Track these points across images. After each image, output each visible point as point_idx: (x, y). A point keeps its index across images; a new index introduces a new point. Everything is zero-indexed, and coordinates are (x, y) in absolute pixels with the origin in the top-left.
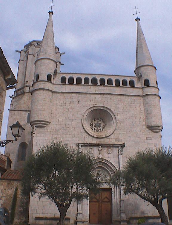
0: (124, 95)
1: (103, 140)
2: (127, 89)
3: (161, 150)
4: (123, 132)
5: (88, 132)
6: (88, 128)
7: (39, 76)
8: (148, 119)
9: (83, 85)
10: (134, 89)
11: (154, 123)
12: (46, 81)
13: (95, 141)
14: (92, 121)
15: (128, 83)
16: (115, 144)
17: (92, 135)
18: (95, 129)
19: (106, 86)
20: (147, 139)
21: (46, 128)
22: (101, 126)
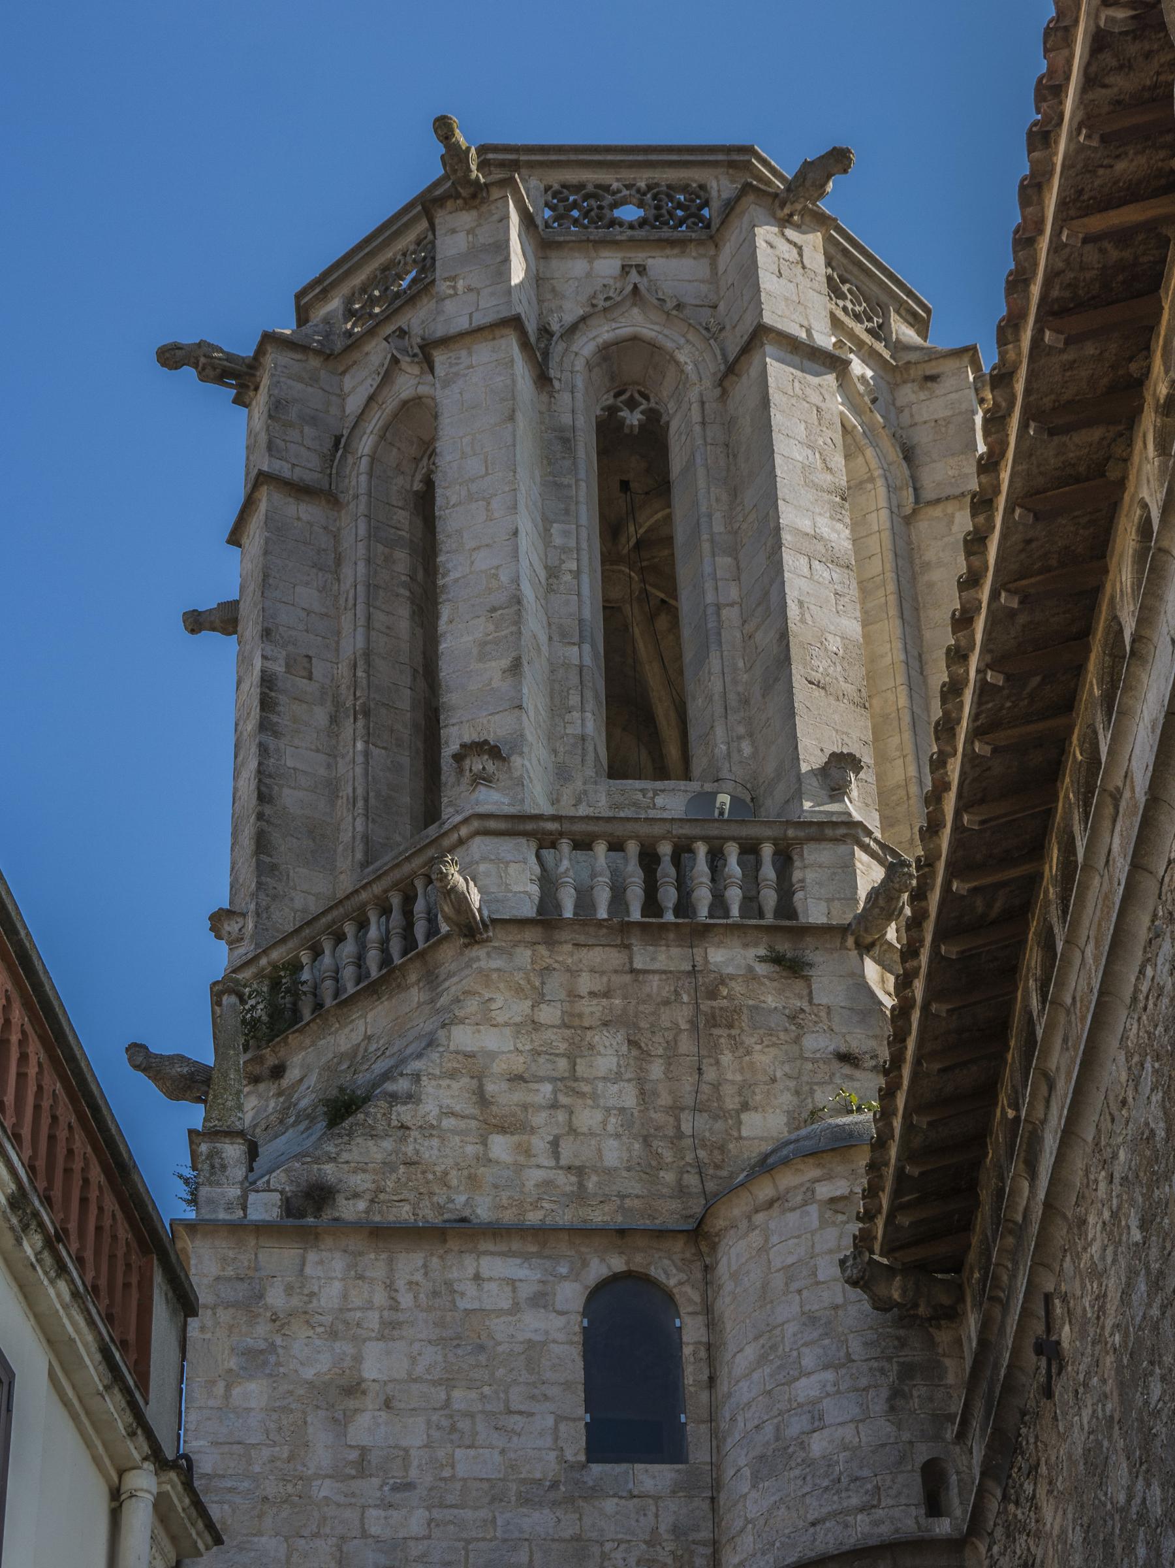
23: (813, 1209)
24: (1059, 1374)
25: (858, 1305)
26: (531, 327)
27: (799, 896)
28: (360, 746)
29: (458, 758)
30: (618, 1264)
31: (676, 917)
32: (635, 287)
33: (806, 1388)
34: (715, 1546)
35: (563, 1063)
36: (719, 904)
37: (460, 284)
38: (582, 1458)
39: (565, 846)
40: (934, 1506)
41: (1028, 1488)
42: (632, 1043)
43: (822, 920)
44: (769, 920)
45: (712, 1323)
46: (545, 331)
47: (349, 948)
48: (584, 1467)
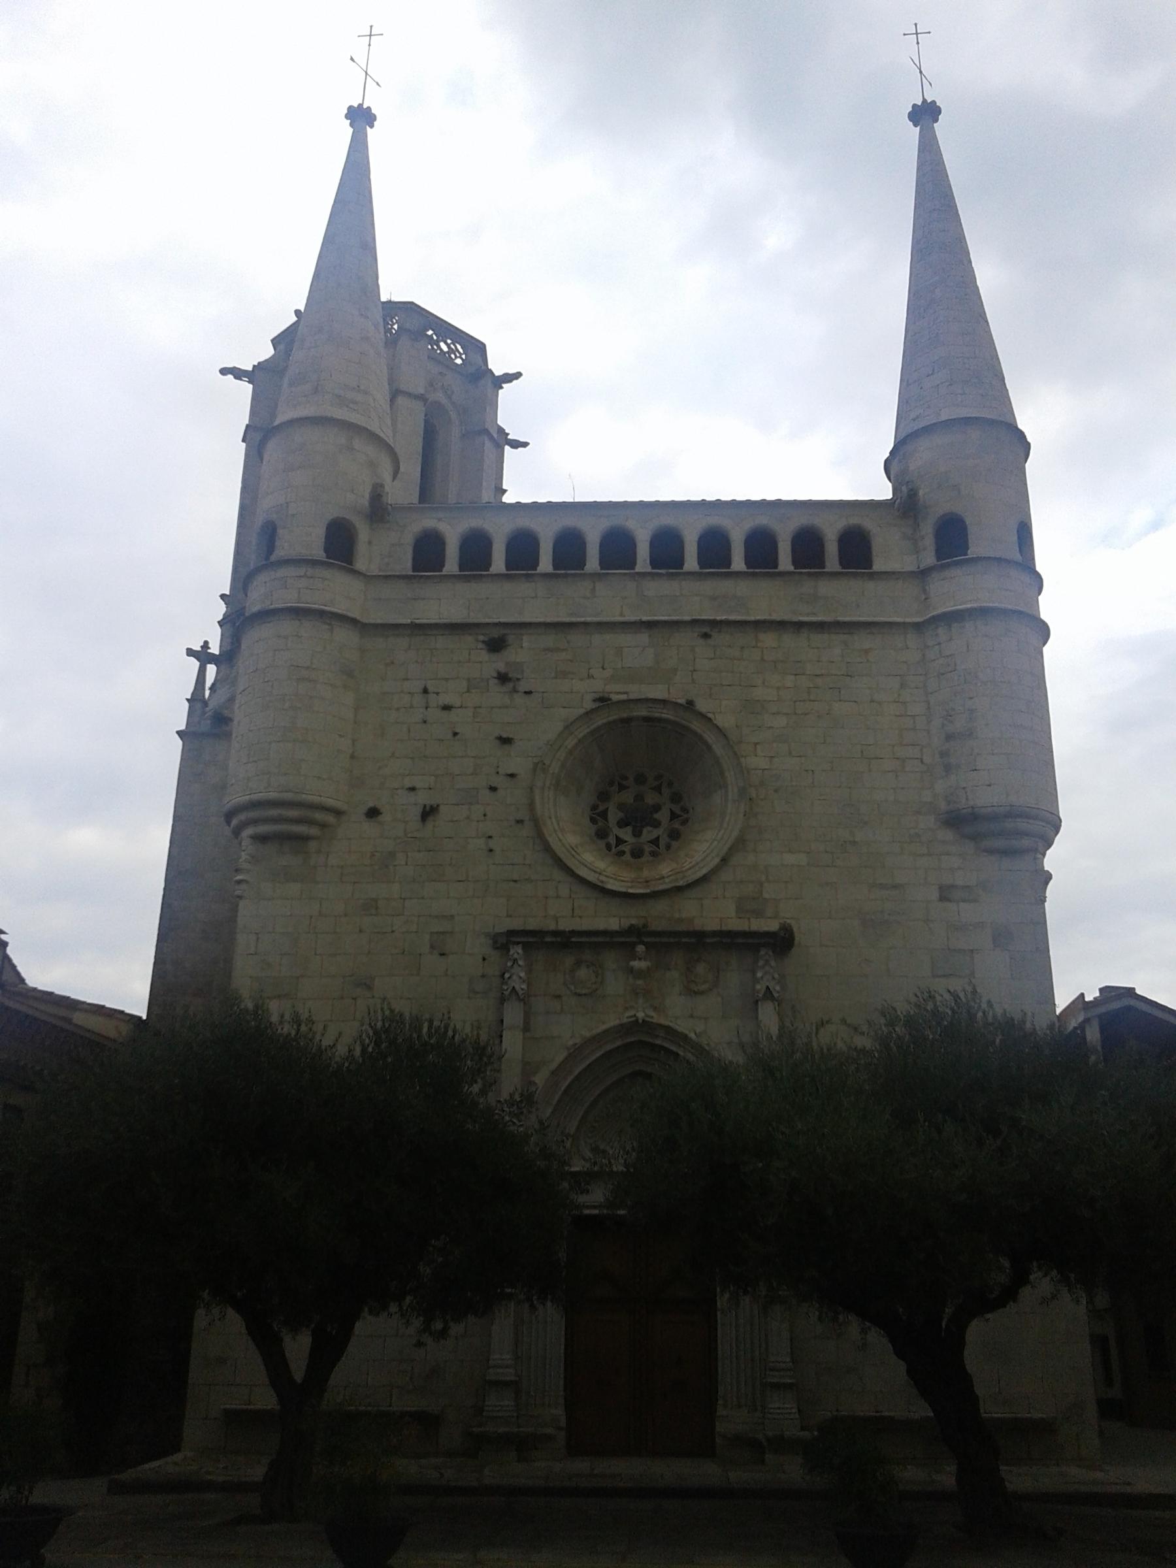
0: (799, 626)
1: (659, 908)
2: (826, 588)
3: (671, 878)
4: (790, 859)
5: (571, 863)
6: (572, 839)
7: (280, 532)
8: (948, 768)
9: (546, 576)
10: (870, 585)
11: (986, 799)
12: (314, 563)
13: (611, 920)
14: (603, 796)
15: (832, 549)
16: (729, 934)
17: (591, 877)
18: (620, 841)
19: (834, 575)
20: (943, 898)
21: (313, 845)
22: (656, 824)
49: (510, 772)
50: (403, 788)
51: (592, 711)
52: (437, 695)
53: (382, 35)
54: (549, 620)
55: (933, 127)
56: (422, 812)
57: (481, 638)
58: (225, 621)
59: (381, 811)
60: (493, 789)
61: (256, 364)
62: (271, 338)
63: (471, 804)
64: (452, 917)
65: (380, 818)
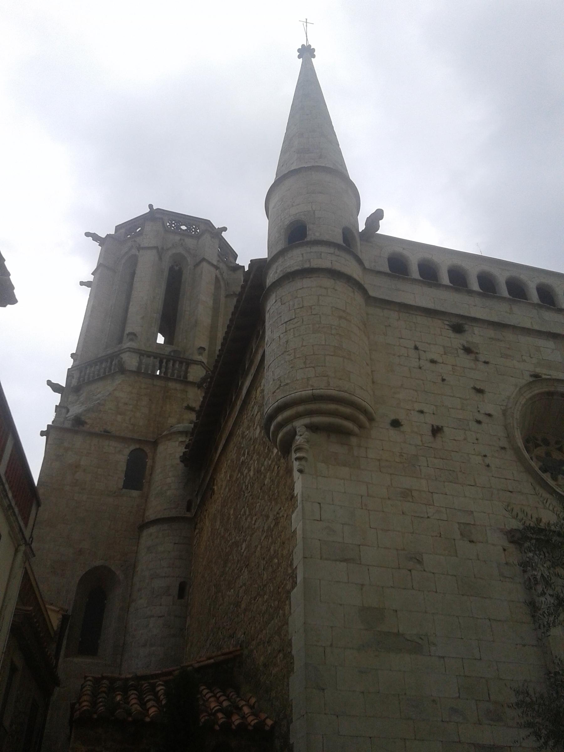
21: (354, 440)
23: (177, 443)
24: (213, 495)
25: (182, 465)
26: (160, 248)
27: (188, 374)
28: (109, 323)
29: (128, 335)
30: (138, 446)
31: (164, 375)
32: (182, 243)
33: (169, 480)
34: (144, 510)
35: (135, 402)
36: (173, 374)
37: (148, 237)
38: (122, 487)
39: (145, 356)
40: (189, 509)
41: (205, 513)
42: (150, 400)
43: (192, 380)
44: (182, 379)
45: (154, 462)
46: (162, 248)
47: (97, 367)
48: (122, 489)
49: (487, 412)
50: (414, 410)
51: (531, 383)
52: (425, 352)
53: (313, 24)
54: (492, 319)
55: (59, 393)
56: (432, 430)
57: (447, 323)
58: (74, 369)
59: (402, 423)
60: (479, 422)
61: (109, 234)
62: (116, 225)
63: (466, 430)
64: (472, 512)
65: (402, 429)
